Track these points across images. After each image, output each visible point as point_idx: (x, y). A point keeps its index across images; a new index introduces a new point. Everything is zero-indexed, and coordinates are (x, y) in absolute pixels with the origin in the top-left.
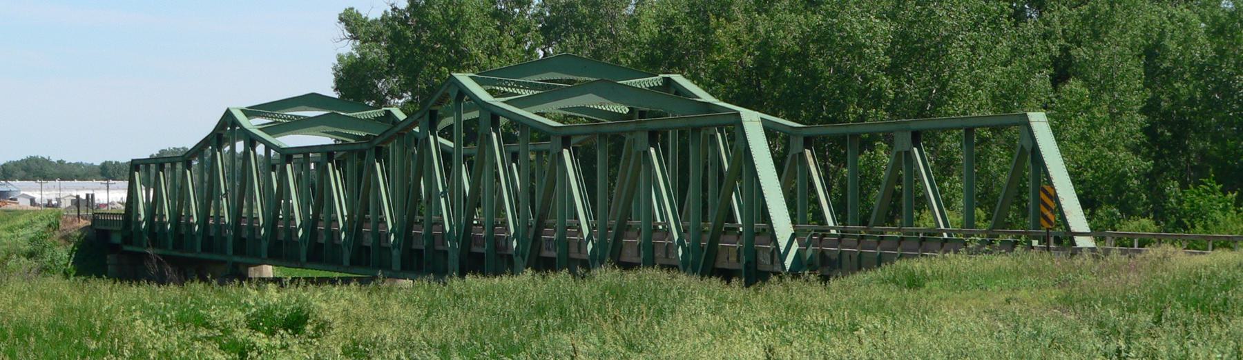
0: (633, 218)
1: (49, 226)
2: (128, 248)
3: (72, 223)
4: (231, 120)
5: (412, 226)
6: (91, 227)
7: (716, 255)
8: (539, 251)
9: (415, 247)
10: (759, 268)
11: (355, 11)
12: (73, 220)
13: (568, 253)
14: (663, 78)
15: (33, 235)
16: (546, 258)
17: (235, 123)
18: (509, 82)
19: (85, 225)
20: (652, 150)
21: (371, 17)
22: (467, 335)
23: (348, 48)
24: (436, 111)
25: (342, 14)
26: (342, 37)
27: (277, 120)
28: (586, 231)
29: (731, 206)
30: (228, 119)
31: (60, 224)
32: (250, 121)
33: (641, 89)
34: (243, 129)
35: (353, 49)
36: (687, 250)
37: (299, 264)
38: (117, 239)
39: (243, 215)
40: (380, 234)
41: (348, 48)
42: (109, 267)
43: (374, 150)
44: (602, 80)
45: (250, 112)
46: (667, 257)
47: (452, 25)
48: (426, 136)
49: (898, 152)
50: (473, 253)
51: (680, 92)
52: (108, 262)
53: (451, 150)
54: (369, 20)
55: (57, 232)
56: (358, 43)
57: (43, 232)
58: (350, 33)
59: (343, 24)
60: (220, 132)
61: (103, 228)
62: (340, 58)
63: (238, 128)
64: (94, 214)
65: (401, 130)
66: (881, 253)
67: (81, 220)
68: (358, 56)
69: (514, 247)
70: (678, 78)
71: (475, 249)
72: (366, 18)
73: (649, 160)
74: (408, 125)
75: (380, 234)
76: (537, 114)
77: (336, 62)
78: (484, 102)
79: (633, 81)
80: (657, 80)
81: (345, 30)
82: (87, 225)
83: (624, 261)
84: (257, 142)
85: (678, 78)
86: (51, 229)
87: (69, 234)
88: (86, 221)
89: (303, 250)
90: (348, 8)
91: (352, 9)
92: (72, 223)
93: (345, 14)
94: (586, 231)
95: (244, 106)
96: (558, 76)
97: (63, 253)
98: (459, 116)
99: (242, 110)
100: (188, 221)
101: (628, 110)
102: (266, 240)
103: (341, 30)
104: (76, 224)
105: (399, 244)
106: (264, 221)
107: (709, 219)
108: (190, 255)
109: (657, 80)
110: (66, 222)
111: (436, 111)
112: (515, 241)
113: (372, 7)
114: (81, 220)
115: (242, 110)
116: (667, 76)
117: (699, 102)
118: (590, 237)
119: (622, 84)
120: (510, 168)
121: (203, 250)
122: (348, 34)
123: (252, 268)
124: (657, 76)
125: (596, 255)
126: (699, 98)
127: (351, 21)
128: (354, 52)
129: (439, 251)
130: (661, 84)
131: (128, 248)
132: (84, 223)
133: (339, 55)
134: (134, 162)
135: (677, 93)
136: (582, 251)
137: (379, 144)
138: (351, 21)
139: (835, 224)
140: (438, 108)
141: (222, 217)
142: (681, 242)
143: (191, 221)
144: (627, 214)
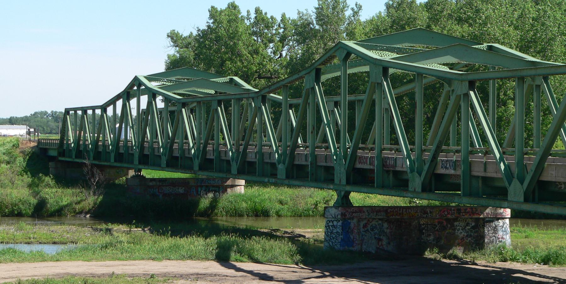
0: (451, 142)
1: (14, 146)
2: (60, 158)
3: (26, 144)
4: (138, 83)
5: (207, 146)
6: (37, 146)
7: (435, 167)
8: (354, 164)
9: (174, 155)
10: (317, 164)
11: (176, 32)
12: (27, 143)
13: (470, 171)
14: (230, 78)
15: (5, 151)
16: (359, 169)
17: (140, 84)
18: (162, 79)
19: (33, 146)
20: (219, 108)
21: (186, 34)
22: (482, 262)
23: (173, 51)
24: (320, 69)
25: (168, 33)
26: (170, 45)
27: (164, 83)
28: (191, 145)
29: (325, 134)
30: (136, 81)
31: (20, 145)
32: (151, 83)
33: (220, 83)
34: (147, 87)
35: (175, 52)
36: (280, 155)
37: (192, 172)
38: (53, 153)
39: (100, 139)
40: (220, 151)
41: (173, 51)
42: (51, 169)
43: (260, 98)
44: (460, 44)
45: (150, 78)
46: (485, 171)
47: (231, 38)
48: (312, 86)
49: (457, 96)
50: (357, 168)
51: (237, 84)
52: (50, 167)
53: (281, 101)
54: (183, 37)
55: (18, 149)
56: (178, 48)
57: (10, 149)
58: (174, 43)
59: (170, 38)
60: (128, 91)
61: (45, 147)
62: (169, 57)
63: (144, 87)
64: (39, 139)
65: (286, 84)
66: (396, 157)
67: (31, 142)
68: (178, 55)
69: (193, 153)
70: (237, 79)
71: (358, 166)
72: (182, 36)
73: (261, 111)
74: (294, 80)
75: (220, 151)
76: (173, 93)
77: (167, 59)
78: (150, 88)
79: (218, 79)
80: (226, 79)
81: (171, 42)
82: (35, 145)
83: (546, 180)
84: (157, 95)
85: (237, 79)
86: (15, 148)
87: (25, 151)
88: (34, 143)
89: (196, 163)
90: (172, 30)
91: (174, 30)
92: (26, 144)
93: (171, 33)
94: (191, 145)
95: (146, 75)
96: (181, 77)
97: (21, 161)
98: (345, 71)
99: (145, 77)
100: (67, 142)
101: (214, 92)
102: (165, 156)
103: (169, 42)
104: (29, 145)
105: (113, 150)
106: (111, 142)
107: (307, 142)
108: (106, 164)
109: (226, 79)
110: (22, 144)
111: (320, 69)
112: (162, 149)
113: (185, 30)
114: (31, 142)
115: (145, 77)
116: (231, 77)
117: (526, 60)
118: (193, 147)
119: (475, 48)
120: (190, 117)
121: (115, 161)
122: (172, 44)
123: (131, 171)
124: (227, 77)
125: (195, 154)
126: (244, 87)
127: (174, 37)
128: (176, 53)
129: (224, 160)
130: (228, 81)
131: (60, 158)
132: (33, 144)
133: (168, 55)
134: (67, 110)
135: (235, 85)
136: (227, 156)
137: (265, 93)
138: (174, 37)
139: (302, 142)
140: (322, 67)
141: (107, 141)
142: (277, 151)
143: (70, 142)
144: (445, 140)
